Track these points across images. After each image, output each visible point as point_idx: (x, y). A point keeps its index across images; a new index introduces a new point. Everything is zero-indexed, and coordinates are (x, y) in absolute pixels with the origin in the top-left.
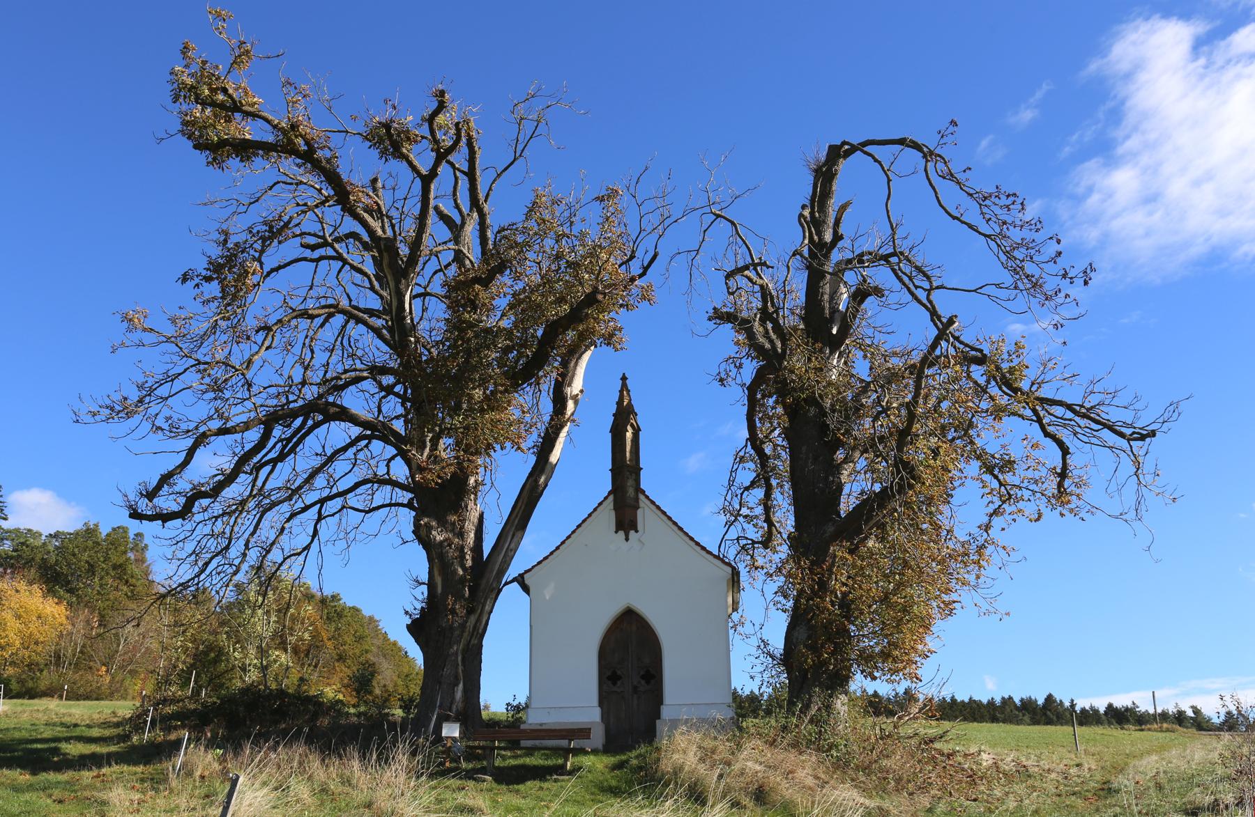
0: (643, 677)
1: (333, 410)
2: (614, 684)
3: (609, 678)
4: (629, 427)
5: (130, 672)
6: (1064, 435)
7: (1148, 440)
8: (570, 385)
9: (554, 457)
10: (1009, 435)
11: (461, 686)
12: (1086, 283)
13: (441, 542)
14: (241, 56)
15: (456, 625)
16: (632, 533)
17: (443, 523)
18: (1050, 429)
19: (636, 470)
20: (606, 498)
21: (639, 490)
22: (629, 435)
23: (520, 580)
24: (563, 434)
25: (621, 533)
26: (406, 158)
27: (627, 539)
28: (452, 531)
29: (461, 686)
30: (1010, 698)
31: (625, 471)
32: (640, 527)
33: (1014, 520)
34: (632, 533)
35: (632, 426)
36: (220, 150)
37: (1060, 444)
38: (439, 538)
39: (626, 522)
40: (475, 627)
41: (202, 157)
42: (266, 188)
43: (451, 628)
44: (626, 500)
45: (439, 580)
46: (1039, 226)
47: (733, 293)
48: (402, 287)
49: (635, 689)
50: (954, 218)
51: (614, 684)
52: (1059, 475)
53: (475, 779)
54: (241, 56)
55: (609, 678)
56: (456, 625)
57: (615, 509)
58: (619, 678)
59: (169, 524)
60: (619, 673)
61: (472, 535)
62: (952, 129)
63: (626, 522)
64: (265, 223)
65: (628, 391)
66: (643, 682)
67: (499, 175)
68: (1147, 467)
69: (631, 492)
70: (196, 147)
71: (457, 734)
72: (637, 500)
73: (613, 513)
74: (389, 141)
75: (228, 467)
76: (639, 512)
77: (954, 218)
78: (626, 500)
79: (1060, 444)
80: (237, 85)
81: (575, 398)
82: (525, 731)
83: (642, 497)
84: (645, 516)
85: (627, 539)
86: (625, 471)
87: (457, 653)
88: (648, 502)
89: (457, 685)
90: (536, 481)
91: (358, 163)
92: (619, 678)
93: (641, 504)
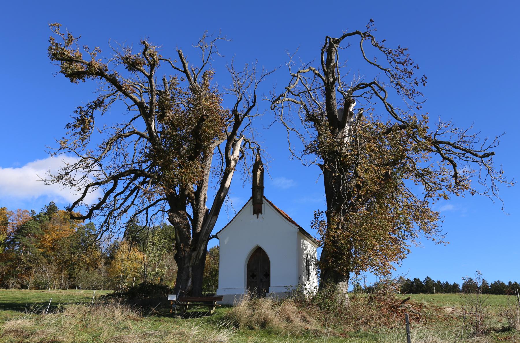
0: (264, 275)
1: (139, 172)
2: (253, 278)
3: (251, 276)
4: (259, 170)
5: (169, 280)
6: (452, 157)
7: (490, 157)
8: (233, 154)
9: (227, 184)
10: (424, 160)
11: (190, 280)
12: (424, 85)
13: (178, 223)
14: (70, 39)
15: (186, 255)
16: (260, 214)
17: (179, 215)
18: (445, 156)
19: (262, 188)
20: (249, 200)
21: (262, 196)
22: (259, 173)
23: (216, 236)
24: (231, 175)
25: (255, 215)
26: (140, 70)
27: (258, 217)
28: (183, 218)
29: (190, 280)
30: (418, 279)
31: (258, 189)
32: (263, 212)
33: (438, 199)
34: (260, 214)
35: (260, 169)
36: (75, 76)
37: (452, 162)
38: (177, 221)
39: (257, 211)
40: (196, 257)
41: (68, 79)
42: (96, 88)
43: (184, 257)
44: (258, 201)
45: (178, 238)
46: (410, 62)
47: (273, 109)
48: (149, 121)
49: (261, 280)
50: (372, 63)
51: (253, 278)
52: (454, 176)
53: (174, 317)
54: (70, 39)
55: (251, 276)
56: (186, 255)
57: (253, 205)
58: (255, 276)
59: (85, 220)
60: (255, 274)
61: (202, 219)
62: (371, 24)
63: (257, 211)
64: (93, 102)
65: (259, 155)
66: (264, 277)
67: (199, 71)
68: (496, 168)
69: (259, 197)
70: (66, 76)
71: (175, 300)
72: (262, 200)
73: (252, 207)
74: (133, 66)
75: (102, 197)
76: (263, 206)
77: (372, 63)
78: (258, 201)
79: (452, 162)
80: (69, 52)
81: (235, 160)
82: (216, 297)
83: (263, 199)
84: (265, 207)
85: (258, 217)
86: (258, 189)
87: (188, 267)
88: (266, 201)
89: (189, 280)
90: (220, 195)
91: (124, 76)
92: (255, 276)
93: (263, 202)
